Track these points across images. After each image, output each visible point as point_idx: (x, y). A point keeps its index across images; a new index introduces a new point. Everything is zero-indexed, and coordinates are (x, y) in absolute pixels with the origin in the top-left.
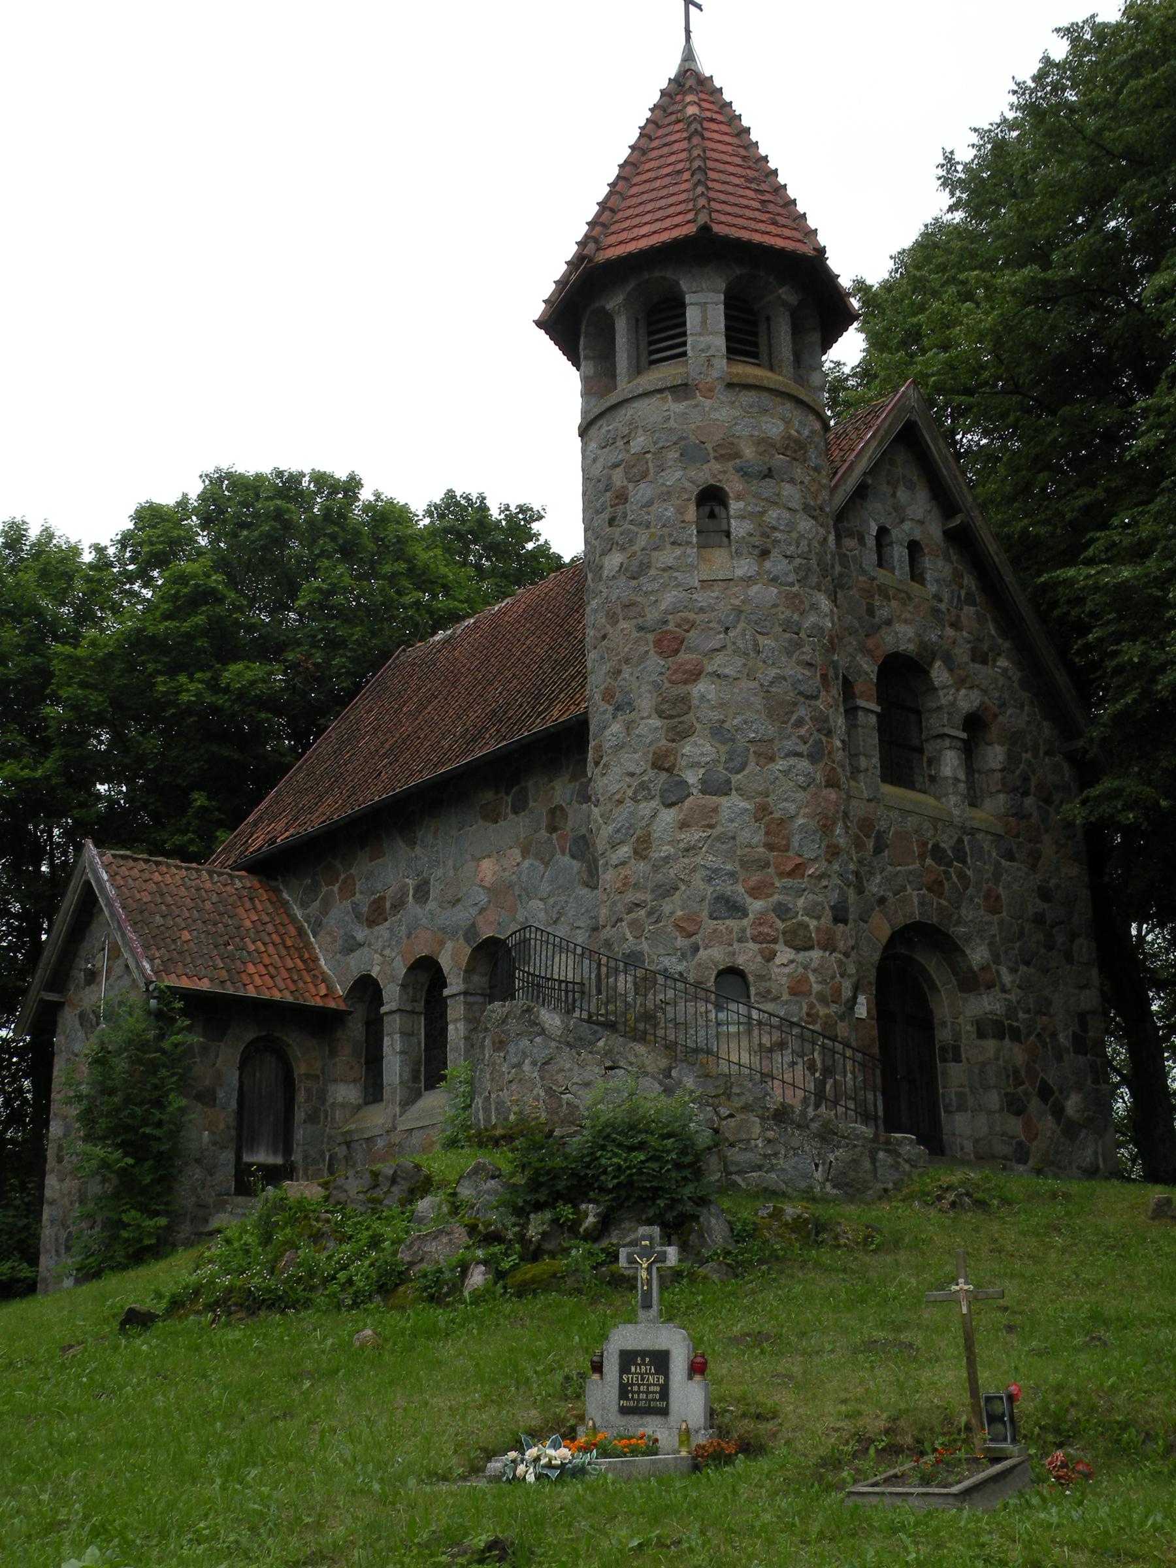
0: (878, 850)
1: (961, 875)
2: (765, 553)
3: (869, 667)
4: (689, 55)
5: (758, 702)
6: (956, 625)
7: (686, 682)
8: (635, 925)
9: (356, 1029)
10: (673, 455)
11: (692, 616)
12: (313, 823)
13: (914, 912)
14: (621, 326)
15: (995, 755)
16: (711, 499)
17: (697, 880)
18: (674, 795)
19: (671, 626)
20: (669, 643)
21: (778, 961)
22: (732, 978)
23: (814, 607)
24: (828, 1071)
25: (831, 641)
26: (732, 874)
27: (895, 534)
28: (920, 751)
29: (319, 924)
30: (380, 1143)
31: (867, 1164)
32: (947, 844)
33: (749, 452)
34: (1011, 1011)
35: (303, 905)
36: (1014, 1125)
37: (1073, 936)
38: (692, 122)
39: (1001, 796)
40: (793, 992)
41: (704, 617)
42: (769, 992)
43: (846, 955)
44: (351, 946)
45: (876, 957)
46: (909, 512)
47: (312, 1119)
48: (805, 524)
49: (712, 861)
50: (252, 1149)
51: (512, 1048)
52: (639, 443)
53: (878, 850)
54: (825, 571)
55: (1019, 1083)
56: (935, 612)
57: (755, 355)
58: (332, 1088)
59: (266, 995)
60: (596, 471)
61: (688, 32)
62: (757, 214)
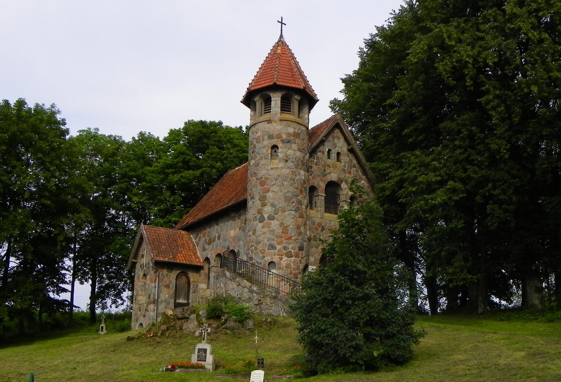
2: (287, 161)
3: (323, 185)
4: (281, 36)
5: (283, 198)
8: (252, 251)
10: (266, 137)
11: (268, 177)
14: (258, 104)
16: (275, 147)
18: (262, 220)
19: (263, 179)
20: (263, 184)
23: (299, 174)
26: (274, 239)
27: (333, 151)
29: (198, 243)
33: (284, 136)
35: (195, 239)
40: (286, 267)
41: (271, 177)
42: (280, 267)
44: (204, 249)
45: (320, 257)
46: (338, 145)
47: (194, 292)
48: (298, 154)
52: (259, 133)
53: (322, 231)
54: (303, 164)
56: (344, 170)
57: (290, 111)
58: (199, 284)
61: (282, 30)
62: (290, 79)
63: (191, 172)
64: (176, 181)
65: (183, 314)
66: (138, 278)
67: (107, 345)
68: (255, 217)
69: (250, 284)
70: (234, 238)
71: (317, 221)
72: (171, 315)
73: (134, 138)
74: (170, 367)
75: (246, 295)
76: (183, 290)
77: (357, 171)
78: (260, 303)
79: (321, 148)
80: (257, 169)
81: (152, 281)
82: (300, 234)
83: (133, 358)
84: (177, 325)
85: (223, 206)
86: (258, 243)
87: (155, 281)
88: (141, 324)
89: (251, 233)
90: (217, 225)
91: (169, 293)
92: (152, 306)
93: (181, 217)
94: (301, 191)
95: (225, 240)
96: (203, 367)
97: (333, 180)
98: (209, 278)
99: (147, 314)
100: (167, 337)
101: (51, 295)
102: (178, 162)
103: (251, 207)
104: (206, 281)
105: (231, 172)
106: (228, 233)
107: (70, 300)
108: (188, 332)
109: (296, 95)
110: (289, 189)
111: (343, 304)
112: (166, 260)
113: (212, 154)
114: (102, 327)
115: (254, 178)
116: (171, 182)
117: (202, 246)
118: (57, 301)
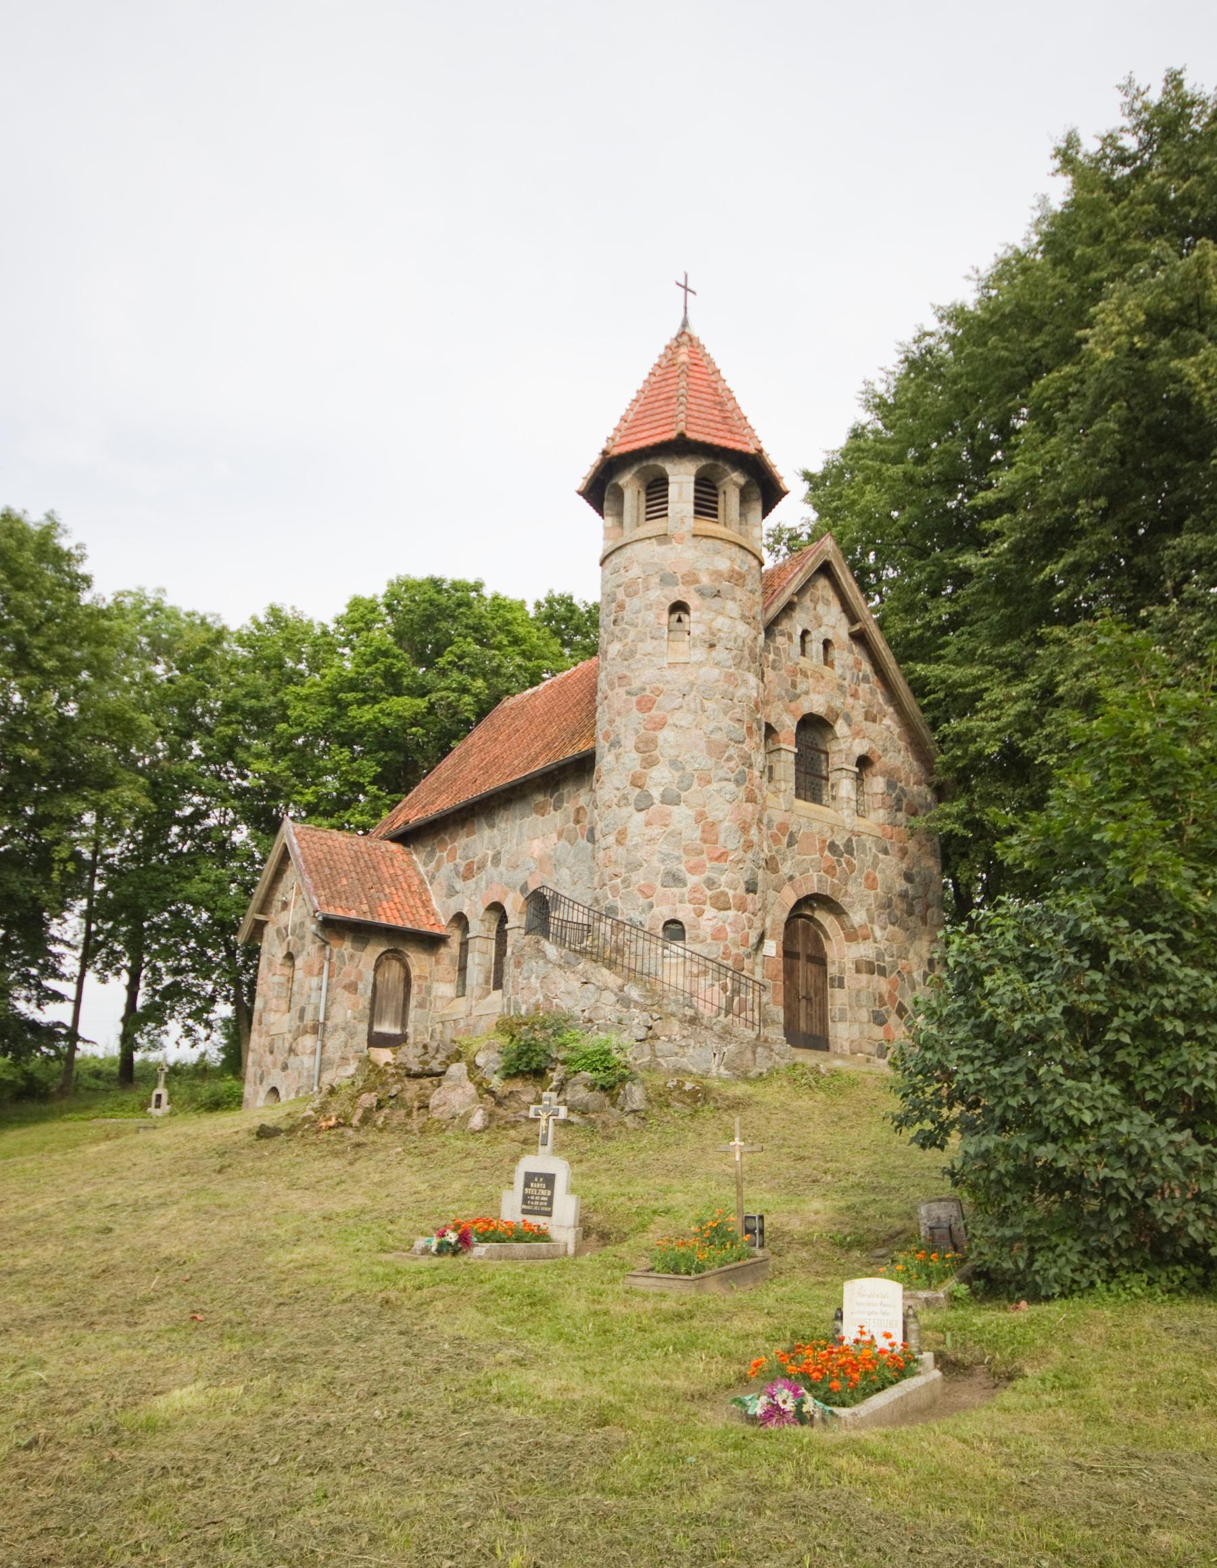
0: (790, 844)
1: (848, 863)
2: (712, 646)
4: (685, 324)
5: (703, 744)
6: (855, 695)
7: (654, 729)
8: (615, 889)
9: (452, 950)
10: (655, 580)
11: (661, 686)
12: (432, 811)
13: (814, 888)
15: (877, 784)
17: (655, 861)
18: (643, 804)
19: (648, 693)
20: (645, 705)
21: (705, 916)
22: (674, 929)
23: (745, 682)
24: (736, 992)
25: (756, 705)
26: (678, 858)
28: (827, 779)
29: (433, 877)
30: (462, 1024)
31: (749, 1055)
32: (840, 842)
33: (705, 580)
34: (880, 956)
35: (425, 864)
36: (878, 1032)
37: (928, 907)
38: (685, 365)
39: (882, 812)
40: (714, 938)
43: (754, 914)
44: (452, 892)
45: (785, 916)
46: (825, 620)
47: (421, 1005)
48: (742, 629)
49: (665, 848)
51: (525, 967)
52: (635, 571)
53: (790, 844)
54: (754, 659)
55: (883, 1004)
57: (716, 516)
58: (435, 985)
59: (393, 923)
60: (608, 590)
63: (406, 699)
64: (369, 721)
65: (425, 1063)
66: (270, 964)
67: (194, 1149)
68: (625, 797)
69: (620, 981)
70: (541, 861)
71: (778, 817)
72: (387, 1064)
73: (255, 620)
74: (452, 1237)
75: (609, 1009)
76: (391, 999)
77: (872, 692)
78: (650, 1037)
79: (785, 625)
80: (628, 667)
81: (310, 972)
82: (749, 845)
83: (293, 1195)
84: (407, 1095)
85: (510, 775)
86: (634, 866)
87: (320, 973)
88: (274, 1091)
89: (611, 839)
90: (492, 826)
91: (355, 1005)
92: (308, 1041)
93: (377, 815)
94: (749, 729)
95: (515, 867)
96: (541, 1236)
97: (814, 711)
98: (463, 969)
99: (293, 1062)
100: (381, 1130)
101: (22, 1006)
102: (373, 675)
103: (612, 770)
104: (455, 976)
105: (508, 702)
106: (527, 847)
107: (69, 1023)
108: (446, 1116)
109: (734, 470)
110: (721, 722)
111: (1147, 1030)
112: (353, 915)
113: (461, 658)
114: (159, 1097)
115: (621, 691)
116: (352, 727)
117: (444, 884)
118: (34, 1026)
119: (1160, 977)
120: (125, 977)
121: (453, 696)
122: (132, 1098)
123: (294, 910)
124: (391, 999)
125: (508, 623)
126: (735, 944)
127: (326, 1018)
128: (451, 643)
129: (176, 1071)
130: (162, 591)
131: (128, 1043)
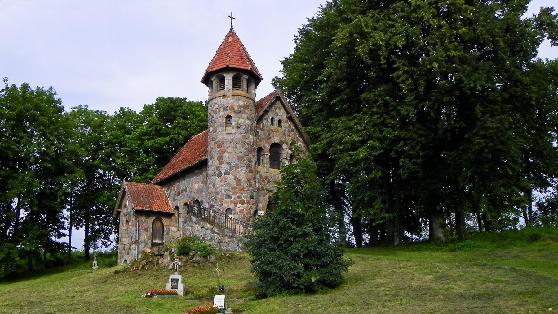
2: (238, 128)
4: (232, 28)
5: (236, 157)
8: (213, 200)
10: (222, 109)
16: (229, 117)
18: (220, 175)
20: (220, 146)
23: (249, 138)
26: (230, 191)
27: (275, 119)
33: (236, 108)
44: (174, 200)
45: (267, 204)
46: (279, 114)
47: (167, 234)
48: (248, 122)
49: (226, 188)
50: (155, 240)
52: (216, 106)
53: (268, 183)
56: (284, 134)
65: (159, 252)
66: (122, 224)
68: (214, 173)
70: (198, 190)
71: (264, 175)
73: (116, 112)
74: (149, 294)
75: (209, 235)
76: (158, 232)
77: (295, 134)
78: (220, 242)
79: (266, 117)
81: (133, 226)
82: (251, 185)
84: (154, 261)
86: (217, 193)
87: (136, 226)
88: (126, 261)
89: (211, 186)
90: (184, 180)
92: (134, 246)
94: (251, 152)
96: (176, 293)
98: (179, 223)
101: (54, 238)
102: (151, 131)
105: (194, 138)
106: (193, 185)
107: (68, 243)
110: (241, 150)
112: (144, 209)
114: (95, 264)
115: (213, 142)
118: (58, 244)
119: (289, 228)
120: (84, 227)
121: (176, 136)
122: (87, 264)
123: (128, 208)
124: (158, 232)
125: (194, 111)
126: (247, 214)
127: (139, 239)
128: (175, 119)
129: (100, 255)
130: (87, 106)
131: (87, 247)
